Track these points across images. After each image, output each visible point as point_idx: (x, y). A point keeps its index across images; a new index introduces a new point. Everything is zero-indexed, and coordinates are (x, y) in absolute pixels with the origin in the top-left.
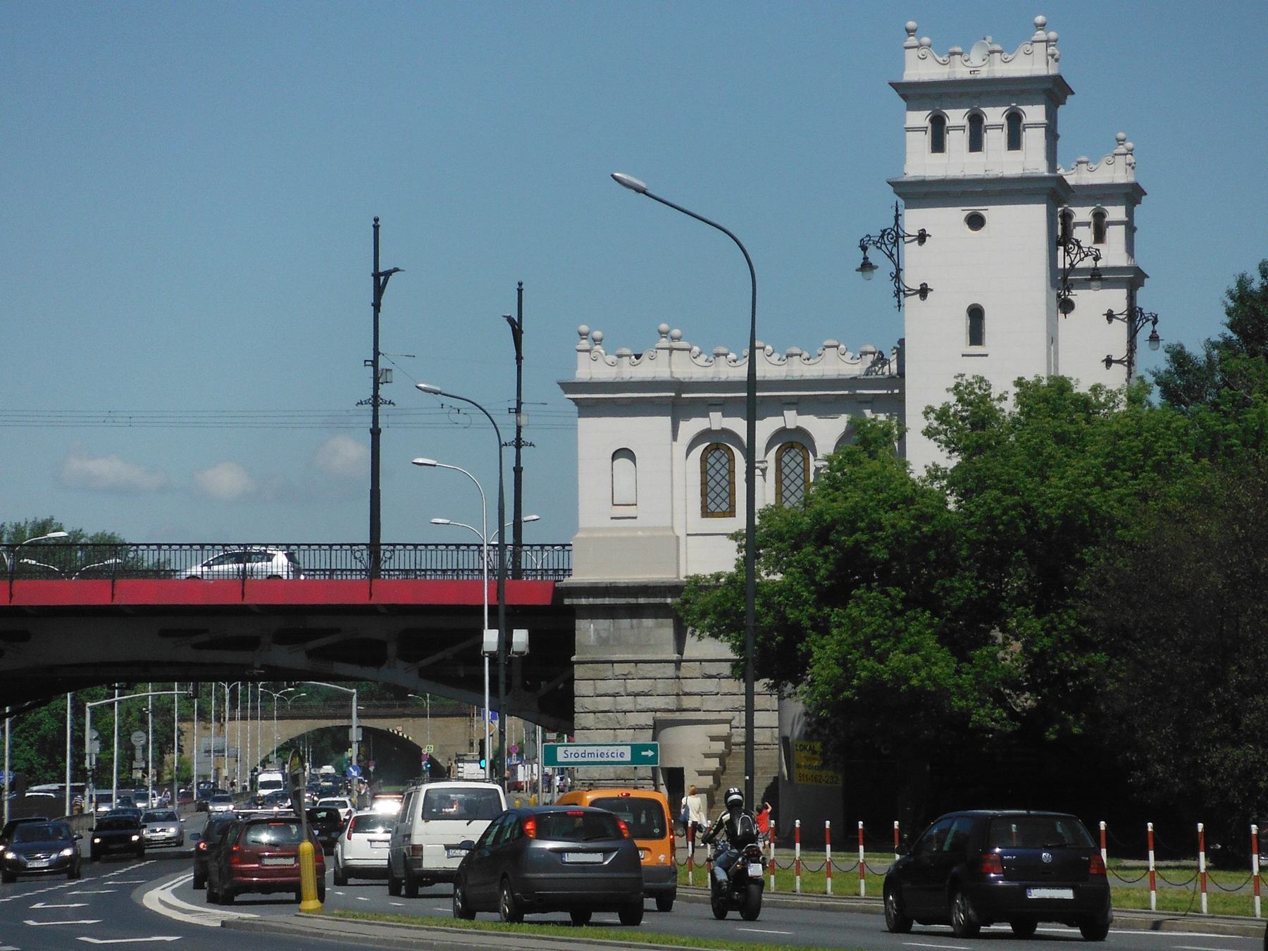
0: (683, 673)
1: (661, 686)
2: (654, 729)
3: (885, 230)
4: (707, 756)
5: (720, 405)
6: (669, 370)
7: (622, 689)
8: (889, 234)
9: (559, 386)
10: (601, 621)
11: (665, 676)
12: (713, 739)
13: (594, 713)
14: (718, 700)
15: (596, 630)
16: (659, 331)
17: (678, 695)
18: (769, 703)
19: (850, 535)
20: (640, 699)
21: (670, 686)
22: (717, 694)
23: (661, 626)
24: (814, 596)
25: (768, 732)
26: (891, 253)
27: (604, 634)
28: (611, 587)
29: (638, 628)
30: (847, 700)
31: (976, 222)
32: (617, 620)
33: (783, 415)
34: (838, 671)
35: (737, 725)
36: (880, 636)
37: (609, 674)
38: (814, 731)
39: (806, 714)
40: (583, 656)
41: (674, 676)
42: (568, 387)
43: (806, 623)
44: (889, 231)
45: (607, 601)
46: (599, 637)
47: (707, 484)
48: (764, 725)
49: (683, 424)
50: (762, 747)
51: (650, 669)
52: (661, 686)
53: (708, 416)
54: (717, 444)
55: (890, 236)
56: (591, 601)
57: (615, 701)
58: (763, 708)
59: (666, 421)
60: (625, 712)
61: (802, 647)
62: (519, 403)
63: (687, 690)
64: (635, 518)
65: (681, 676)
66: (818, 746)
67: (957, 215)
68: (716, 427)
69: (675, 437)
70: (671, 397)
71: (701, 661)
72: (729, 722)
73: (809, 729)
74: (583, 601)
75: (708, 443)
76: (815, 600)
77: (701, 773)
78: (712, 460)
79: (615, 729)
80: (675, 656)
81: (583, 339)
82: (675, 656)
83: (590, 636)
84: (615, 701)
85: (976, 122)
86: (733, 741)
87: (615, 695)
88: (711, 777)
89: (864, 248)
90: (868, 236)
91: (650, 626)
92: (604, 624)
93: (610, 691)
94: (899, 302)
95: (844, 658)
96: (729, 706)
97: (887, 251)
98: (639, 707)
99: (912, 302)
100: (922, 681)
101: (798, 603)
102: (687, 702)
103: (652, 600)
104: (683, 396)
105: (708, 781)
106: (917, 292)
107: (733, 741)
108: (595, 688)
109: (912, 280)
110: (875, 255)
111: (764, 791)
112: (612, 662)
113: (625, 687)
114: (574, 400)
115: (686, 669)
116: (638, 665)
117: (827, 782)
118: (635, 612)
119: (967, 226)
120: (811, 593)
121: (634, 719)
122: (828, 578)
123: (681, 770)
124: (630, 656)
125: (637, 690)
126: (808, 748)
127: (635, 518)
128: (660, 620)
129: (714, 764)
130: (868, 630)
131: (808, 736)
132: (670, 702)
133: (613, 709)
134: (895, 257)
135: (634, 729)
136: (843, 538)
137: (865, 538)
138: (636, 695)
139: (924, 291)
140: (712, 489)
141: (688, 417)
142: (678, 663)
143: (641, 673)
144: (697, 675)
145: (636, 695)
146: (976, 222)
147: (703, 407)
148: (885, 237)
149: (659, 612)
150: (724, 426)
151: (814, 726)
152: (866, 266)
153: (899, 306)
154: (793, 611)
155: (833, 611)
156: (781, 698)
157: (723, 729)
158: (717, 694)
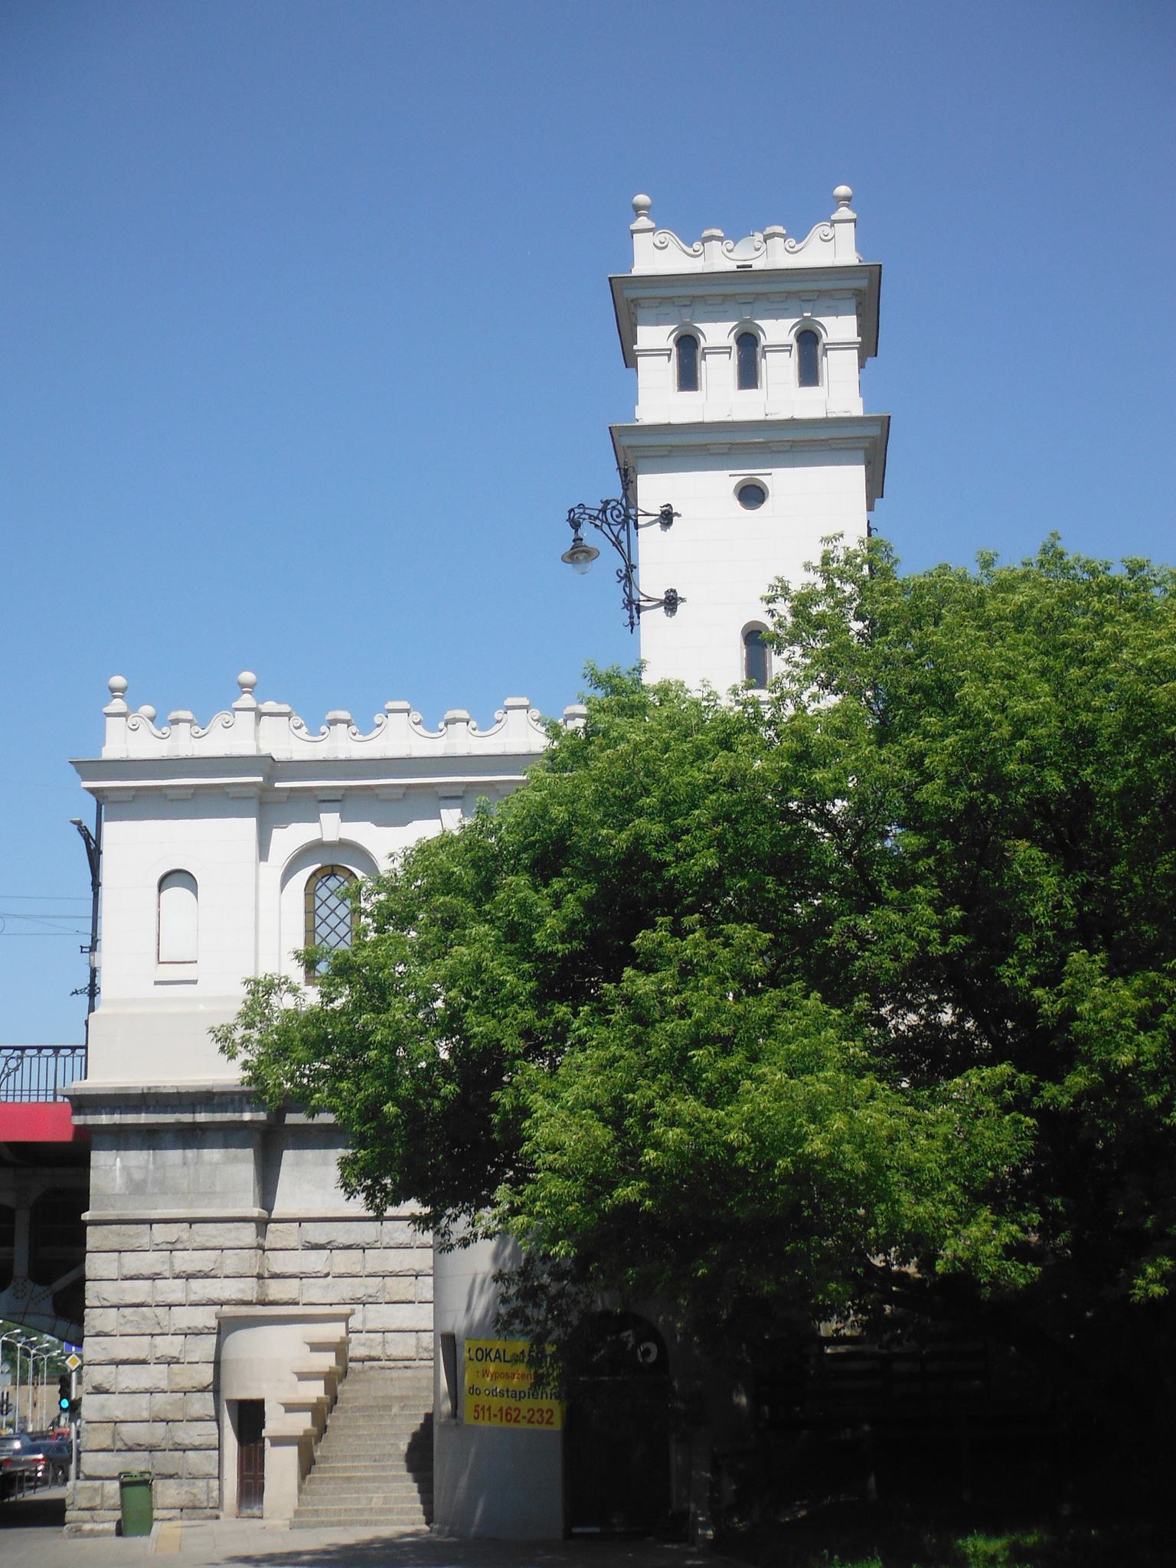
0: (270, 1241)
1: (232, 1262)
2: (219, 1333)
3: (607, 502)
4: (303, 1376)
5: (338, 801)
6: (254, 743)
7: (166, 1267)
8: (614, 508)
9: (72, 767)
10: (132, 1153)
11: (241, 1244)
12: (316, 1347)
13: (118, 1307)
14: (328, 1286)
15: (124, 1168)
16: (239, 683)
17: (260, 1277)
18: (413, 1291)
19: (622, 827)
20: (195, 1284)
21: (248, 1261)
22: (327, 1275)
23: (235, 1160)
24: (532, 985)
25: (411, 1338)
26: (617, 538)
27: (138, 1176)
28: (149, 1094)
29: (196, 1163)
30: (629, 1209)
31: (752, 495)
32: (158, 1152)
33: (440, 817)
34: (603, 1134)
35: (360, 1327)
36: (710, 1040)
37: (145, 1241)
38: (514, 1314)
39: (499, 1277)
40: (101, 1212)
41: (255, 1245)
42: (89, 768)
43: (513, 1043)
44: (613, 504)
45: (143, 1118)
46: (129, 1179)
47: (314, 931)
48: (404, 1326)
49: (277, 834)
50: (400, 1364)
51: (215, 1232)
52: (232, 1262)
53: (316, 819)
54: (332, 866)
55: (616, 513)
56: (117, 1118)
57: (154, 1287)
58: (403, 1298)
59: (248, 826)
60: (170, 1306)
61: (504, 1098)
62: (95, 940)
63: (277, 1270)
64: (195, 982)
65: (267, 1245)
66: (521, 1345)
67: (723, 482)
68: (330, 836)
69: (263, 852)
70: (254, 784)
71: (300, 1221)
72: (345, 1318)
73: (503, 1310)
74: (104, 1119)
75: (319, 865)
76: (532, 994)
77: (291, 1408)
78: (323, 893)
79: (152, 1335)
80: (256, 1211)
81: (116, 697)
82: (256, 1211)
83: (114, 1179)
84: (154, 1287)
85: (748, 344)
86: (351, 1354)
87: (154, 1277)
88: (309, 1415)
89: (576, 525)
90: (581, 506)
91: (215, 1160)
92: (138, 1159)
93: (146, 1272)
94: (631, 617)
95: (617, 1102)
96: (347, 1295)
97: (611, 536)
98: (193, 1298)
99: (652, 620)
100: (836, 1143)
101: (494, 999)
102: (277, 1290)
103: (219, 1117)
104: (277, 785)
105: (303, 1422)
106: (662, 603)
107: (351, 1354)
108: (121, 1266)
109: (651, 583)
110: (589, 534)
111: (407, 1440)
112: (151, 1222)
113: (172, 1263)
114: (92, 791)
115: (276, 1234)
116: (195, 1226)
117: (530, 1421)
118: (191, 1137)
119: (738, 502)
120: (522, 976)
121: (185, 1318)
122: (566, 937)
123: (260, 1404)
124: (182, 1211)
125: (190, 1268)
126: (493, 1355)
127: (195, 982)
128: (232, 1151)
129: (315, 1391)
130: (679, 1026)
131: (503, 1323)
132: (247, 1289)
133: (149, 1301)
134: (625, 545)
135: (186, 1335)
136: (604, 832)
137: (657, 829)
138: (189, 1277)
139: (671, 602)
140: (324, 902)
141: (284, 822)
142: (262, 1224)
143: (199, 1241)
144: (293, 1245)
145: (189, 1277)
146: (752, 495)
147: (310, 805)
148: (608, 512)
149: (228, 1136)
150: (343, 837)
151: (516, 1303)
152: (579, 553)
153: (632, 624)
154: (482, 1019)
155: (576, 1014)
156: (443, 1248)
157: (334, 1332)
158: (327, 1275)
